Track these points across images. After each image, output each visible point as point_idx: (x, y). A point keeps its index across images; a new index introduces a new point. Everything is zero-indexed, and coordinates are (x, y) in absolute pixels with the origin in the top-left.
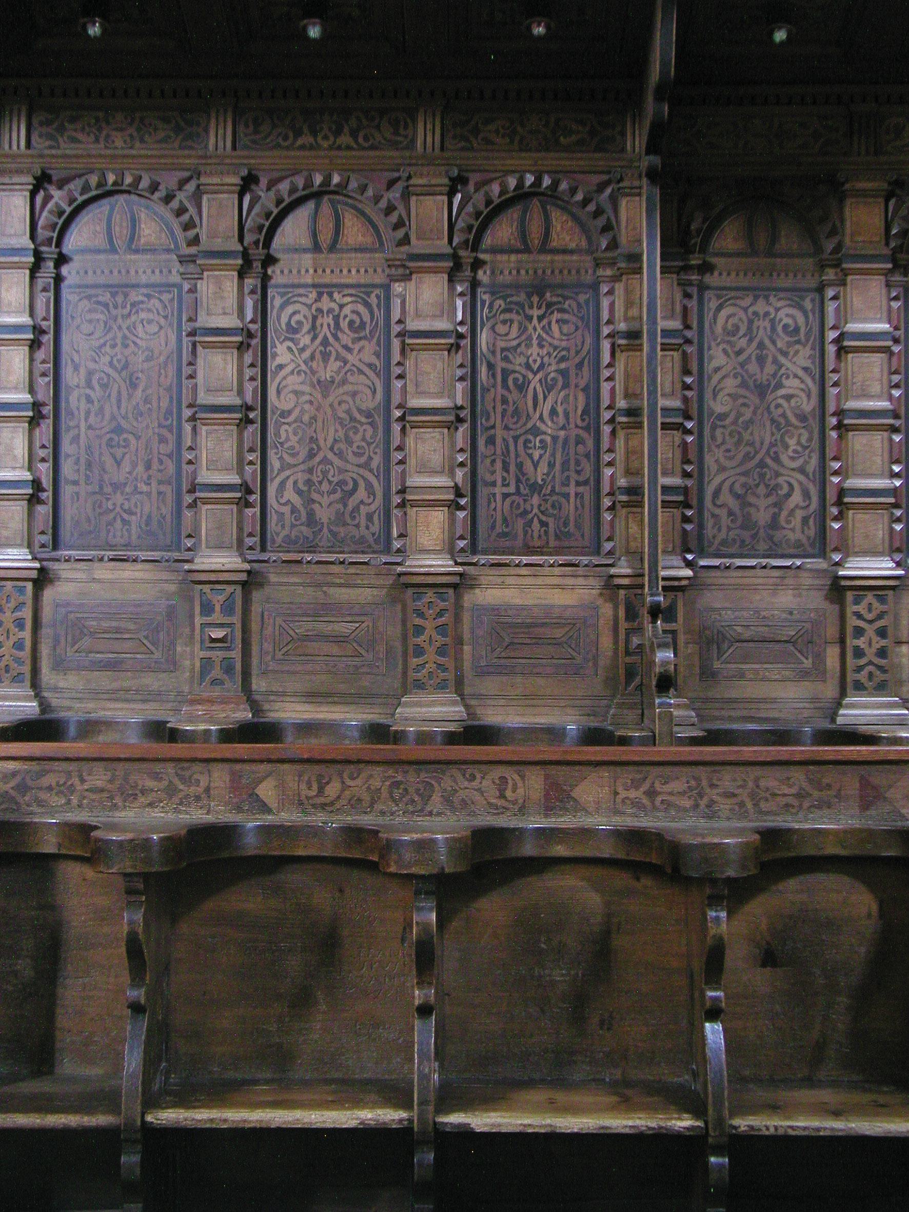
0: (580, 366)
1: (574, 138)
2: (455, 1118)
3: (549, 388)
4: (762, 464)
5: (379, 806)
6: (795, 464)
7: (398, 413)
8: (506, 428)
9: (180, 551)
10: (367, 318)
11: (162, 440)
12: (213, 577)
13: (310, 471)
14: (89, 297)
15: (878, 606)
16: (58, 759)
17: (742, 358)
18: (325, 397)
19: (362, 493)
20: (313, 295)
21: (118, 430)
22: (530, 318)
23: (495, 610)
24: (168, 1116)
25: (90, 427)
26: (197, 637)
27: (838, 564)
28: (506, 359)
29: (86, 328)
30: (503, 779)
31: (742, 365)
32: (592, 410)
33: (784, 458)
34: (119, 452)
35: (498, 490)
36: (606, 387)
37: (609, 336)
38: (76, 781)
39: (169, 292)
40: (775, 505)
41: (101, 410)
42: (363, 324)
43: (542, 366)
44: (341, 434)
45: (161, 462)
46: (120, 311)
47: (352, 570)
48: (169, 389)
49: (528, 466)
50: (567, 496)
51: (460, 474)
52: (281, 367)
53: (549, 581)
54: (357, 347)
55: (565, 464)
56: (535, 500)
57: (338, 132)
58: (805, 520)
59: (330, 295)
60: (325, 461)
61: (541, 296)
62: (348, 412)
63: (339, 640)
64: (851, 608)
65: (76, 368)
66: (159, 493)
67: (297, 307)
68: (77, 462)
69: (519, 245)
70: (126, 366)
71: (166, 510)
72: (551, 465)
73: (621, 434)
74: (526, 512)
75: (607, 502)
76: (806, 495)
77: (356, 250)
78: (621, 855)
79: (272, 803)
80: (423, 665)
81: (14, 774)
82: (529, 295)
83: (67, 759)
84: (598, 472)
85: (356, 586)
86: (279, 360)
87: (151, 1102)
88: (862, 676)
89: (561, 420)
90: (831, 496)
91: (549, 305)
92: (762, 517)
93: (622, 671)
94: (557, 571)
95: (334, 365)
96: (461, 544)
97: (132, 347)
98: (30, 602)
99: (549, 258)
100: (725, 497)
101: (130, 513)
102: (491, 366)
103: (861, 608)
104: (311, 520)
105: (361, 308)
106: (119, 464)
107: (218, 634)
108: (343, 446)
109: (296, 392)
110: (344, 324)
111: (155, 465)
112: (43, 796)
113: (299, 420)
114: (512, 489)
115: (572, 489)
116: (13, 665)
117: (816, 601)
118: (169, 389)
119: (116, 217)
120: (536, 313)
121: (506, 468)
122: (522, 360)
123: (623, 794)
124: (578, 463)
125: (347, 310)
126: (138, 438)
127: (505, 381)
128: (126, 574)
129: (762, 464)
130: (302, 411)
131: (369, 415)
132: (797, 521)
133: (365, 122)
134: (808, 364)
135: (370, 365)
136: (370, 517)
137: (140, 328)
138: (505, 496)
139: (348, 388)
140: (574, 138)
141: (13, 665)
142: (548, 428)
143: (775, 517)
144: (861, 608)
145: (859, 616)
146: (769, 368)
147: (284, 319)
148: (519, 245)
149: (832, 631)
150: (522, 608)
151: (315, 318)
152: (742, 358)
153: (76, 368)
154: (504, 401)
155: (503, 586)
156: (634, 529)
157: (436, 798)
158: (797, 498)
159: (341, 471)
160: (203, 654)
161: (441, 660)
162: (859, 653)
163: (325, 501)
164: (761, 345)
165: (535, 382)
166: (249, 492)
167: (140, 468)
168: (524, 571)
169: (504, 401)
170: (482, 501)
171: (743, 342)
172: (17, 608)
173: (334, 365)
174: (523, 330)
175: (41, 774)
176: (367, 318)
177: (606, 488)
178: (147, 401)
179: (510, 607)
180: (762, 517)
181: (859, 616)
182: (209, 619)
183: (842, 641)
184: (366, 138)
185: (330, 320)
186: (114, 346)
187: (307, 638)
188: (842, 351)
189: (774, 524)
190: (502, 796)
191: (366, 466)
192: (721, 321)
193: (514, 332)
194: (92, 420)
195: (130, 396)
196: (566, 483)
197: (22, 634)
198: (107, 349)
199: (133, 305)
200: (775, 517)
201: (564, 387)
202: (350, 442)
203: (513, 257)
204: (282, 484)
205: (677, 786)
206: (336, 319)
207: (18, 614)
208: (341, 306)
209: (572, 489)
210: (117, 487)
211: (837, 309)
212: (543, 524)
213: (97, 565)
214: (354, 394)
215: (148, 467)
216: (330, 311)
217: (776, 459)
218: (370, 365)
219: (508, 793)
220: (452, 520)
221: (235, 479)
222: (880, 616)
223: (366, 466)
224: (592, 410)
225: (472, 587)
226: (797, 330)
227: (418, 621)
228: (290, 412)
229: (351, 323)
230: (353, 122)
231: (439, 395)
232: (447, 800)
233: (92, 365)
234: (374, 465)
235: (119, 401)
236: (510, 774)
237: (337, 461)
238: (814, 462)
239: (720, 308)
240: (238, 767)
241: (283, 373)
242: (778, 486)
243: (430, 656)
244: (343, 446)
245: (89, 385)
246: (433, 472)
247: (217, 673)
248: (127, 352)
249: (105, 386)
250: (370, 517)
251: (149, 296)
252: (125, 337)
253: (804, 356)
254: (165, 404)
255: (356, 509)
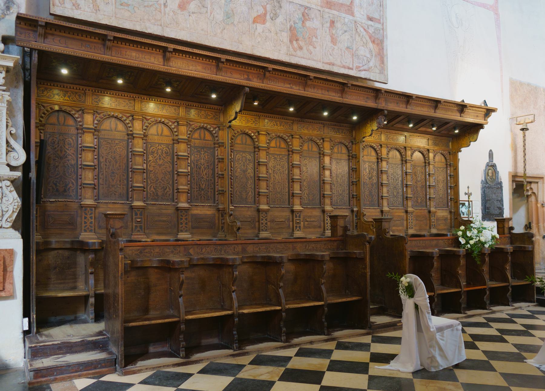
0: (211, 164)
1: (211, 117)
2: (241, 311)
3: (205, 169)
4: (244, 186)
5: (212, 253)
6: (250, 187)
7: (130, 170)
8: (197, 177)
9: (77, 199)
10: (168, 151)
11: (123, 175)
12: (138, 207)
13: (157, 184)
14: (106, 141)
15: (265, 215)
16: (148, 246)
17: (156, 158)
18: (160, 168)
19: (168, 189)
20: (157, 145)
21: (113, 173)
22: (201, 154)
23: (195, 215)
24: (190, 317)
25: (106, 172)
26: (134, 221)
27: (292, 207)
28: (197, 162)
29: (105, 148)
30: (235, 247)
31: (156, 160)
32: (214, 173)
33: (248, 185)
34: (113, 178)
35: (196, 190)
36: (216, 170)
37: (217, 159)
38: (152, 251)
39: (47, 135)
40: (247, 194)
41: (109, 168)
42: (168, 153)
43: (204, 164)
44: (163, 176)
45: (123, 181)
46: (113, 145)
47: (166, 206)
48: (125, 164)
49: (201, 185)
50: (208, 191)
51: (189, 186)
52: (150, 161)
53: (206, 209)
54: (166, 157)
55: (208, 185)
56: (203, 192)
57: (281, 126)
58: (252, 198)
59: (161, 145)
60: (160, 182)
61: (204, 149)
62: (165, 171)
63: (164, 221)
64: (261, 215)
65: (103, 158)
66: (123, 188)
67: (154, 147)
68: (103, 180)
69: (199, 138)
70: (115, 158)
71: (125, 192)
72: (206, 185)
73: (219, 179)
74: (201, 195)
75: (217, 193)
76: (252, 192)
77: (166, 136)
78: (251, 261)
79: (192, 254)
80: (182, 227)
81: (139, 250)
82: (201, 149)
83: (150, 246)
84: (128, 183)
85: (167, 210)
86: (150, 159)
87: (240, 307)
88: (263, 228)
89: (207, 175)
90: (256, 193)
91: (205, 151)
92: (244, 197)
93: (221, 227)
94: (207, 207)
95: (162, 161)
96: (189, 201)
97: (116, 154)
98: (93, 213)
99: (205, 141)
100: (238, 193)
101: (116, 192)
102: (194, 164)
103: (263, 215)
104: (157, 195)
105: (167, 149)
106: (113, 181)
107: (139, 220)
108: (163, 179)
109: (154, 166)
110: (164, 152)
111: (122, 181)
112: (145, 254)
113: (154, 173)
114: (198, 190)
115: (210, 190)
116: (90, 227)
117: (255, 214)
118: (125, 164)
119: (112, 123)
120: (202, 153)
121: (197, 185)
122: (200, 162)
123: (255, 249)
124: (123, 181)
125: (164, 149)
126: (118, 175)
127: (196, 167)
128: (116, 206)
129: (244, 186)
130: (155, 171)
131: (169, 172)
132: (250, 198)
133: (72, 95)
134: (252, 167)
135: (169, 162)
136: (169, 195)
137: (118, 149)
138: (197, 191)
139: (165, 166)
140: (211, 117)
141: (90, 227)
142: (205, 177)
143: (246, 197)
144: (263, 215)
145: (262, 216)
146: (245, 167)
147: (151, 150)
148: (199, 138)
149: (257, 220)
150: (201, 214)
151: (158, 150)
152: (156, 158)
153: (103, 158)
154: (197, 171)
155: (197, 210)
156: (222, 199)
157: (223, 251)
158: (250, 193)
159: (163, 184)
160: (135, 225)
161: (186, 226)
162: (262, 223)
163: (160, 191)
164: (244, 163)
165: (202, 167)
166: (144, 188)
167: (118, 182)
168: (201, 207)
169: (197, 171)
170: (192, 192)
171: (156, 155)
172: (91, 214)
173: (162, 161)
174: (200, 156)
175: (144, 249)
176: (168, 151)
177: (216, 190)
178: (120, 166)
179: (198, 214)
180: (244, 197)
181: (262, 216)
182: (137, 217)
183: (259, 221)
184: (72, 99)
185: (161, 151)
186: (112, 153)
187: (156, 221)
188: (178, 159)
189: (246, 198)
190: (234, 250)
191: (168, 183)
192: (237, 157)
193: (198, 157)
194: (107, 170)
195: (116, 165)
196: (208, 189)
197: (92, 220)
198: (110, 153)
199: (116, 144)
200: (246, 197)
201: (208, 169)
202: (165, 178)
203: (198, 141)
204: (151, 187)
205: (264, 247)
206: (162, 151)
207: (91, 215)
208: (163, 148)
209: (210, 190)
210: (113, 186)
211: (81, 140)
212: (204, 197)
213: (109, 204)
214: (166, 168)
215: (120, 181)
216: (161, 149)
217: (247, 185)
218: (169, 162)
219: (236, 250)
220: (188, 196)
221: (93, 182)
222: (266, 216)
223: (168, 183)
224: (214, 173)
225: (191, 210)
226: (250, 160)
227: (181, 217)
228: (152, 171)
229: (165, 152)
230: (69, 94)
231: (185, 169)
232: (225, 252)
233: (106, 157)
234: (170, 183)
235: (113, 166)
236: (236, 246)
237: (163, 182)
238: (253, 186)
239: (237, 155)
240: (185, 246)
241: (151, 162)
242: (247, 191)
243: (184, 225)
244: (163, 179)
245: (106, 162)
246: (184, 185)
247: (138, 229)
248: (115, 154)
249: (110, 162)
250: (169, 195)
251: (120, 142)
252: (114, 151)
253: (251, 165)
254: (124, 167)
255: (167, 193)
